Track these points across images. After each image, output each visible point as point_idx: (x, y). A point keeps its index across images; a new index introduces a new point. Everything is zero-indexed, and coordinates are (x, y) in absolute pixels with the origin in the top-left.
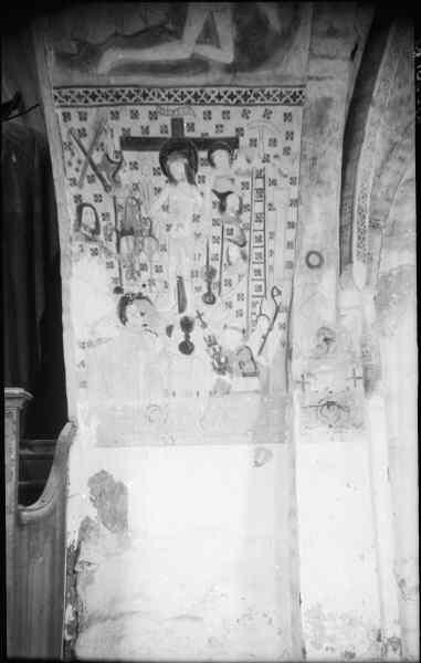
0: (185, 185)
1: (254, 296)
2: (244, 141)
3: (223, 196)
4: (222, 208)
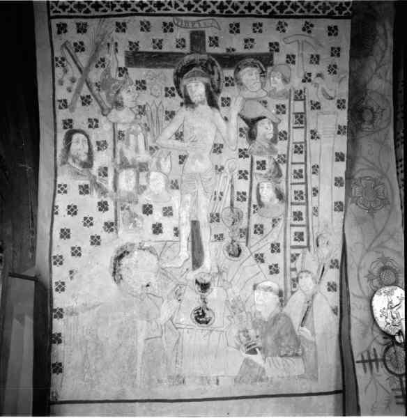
0: (205, 108)
1: (294, 184)
2: (279, 58)
3: (252, 123)
4: (252, 136)
